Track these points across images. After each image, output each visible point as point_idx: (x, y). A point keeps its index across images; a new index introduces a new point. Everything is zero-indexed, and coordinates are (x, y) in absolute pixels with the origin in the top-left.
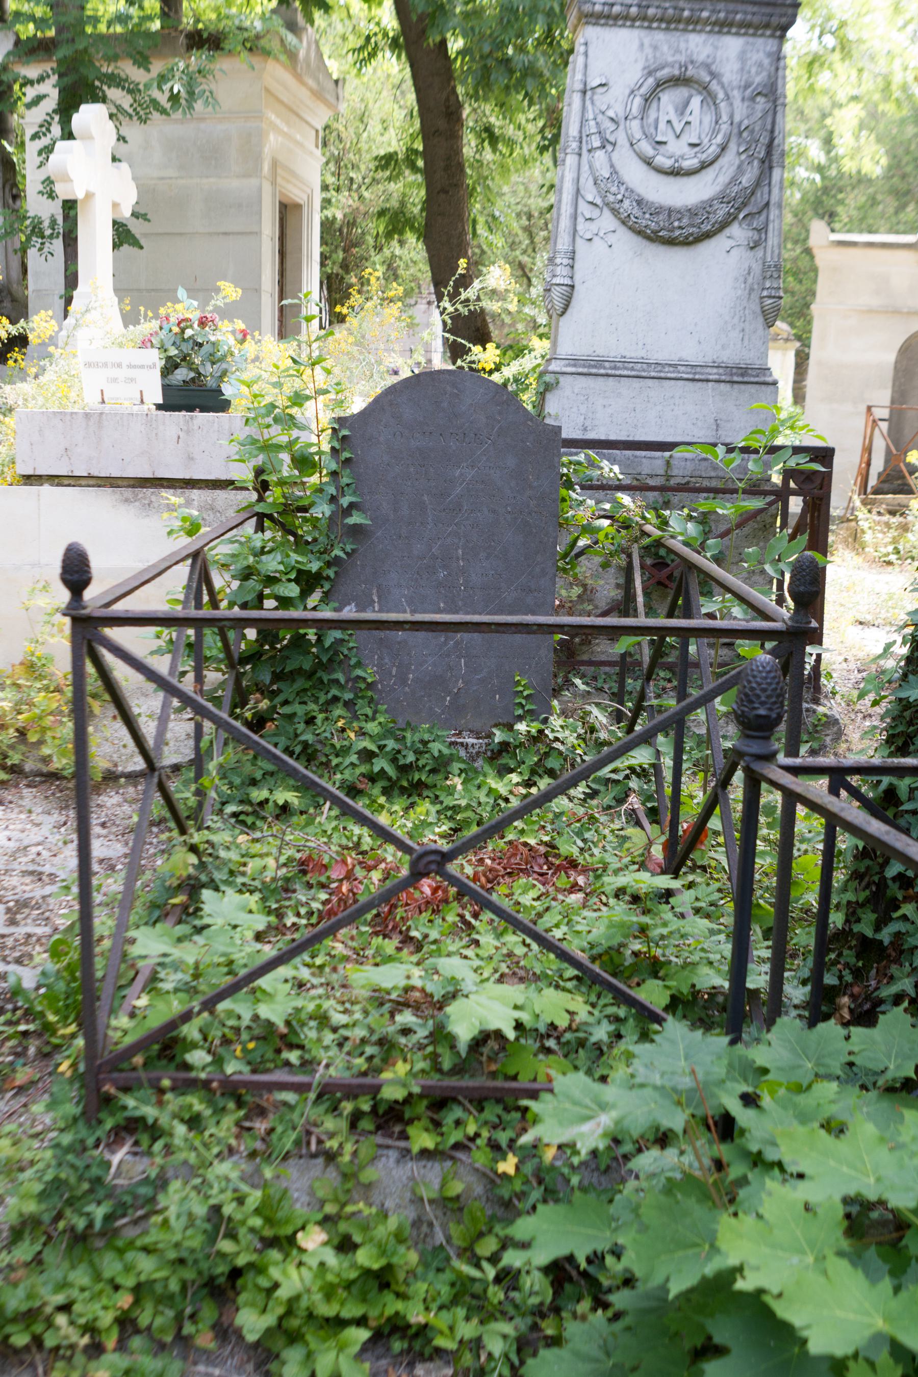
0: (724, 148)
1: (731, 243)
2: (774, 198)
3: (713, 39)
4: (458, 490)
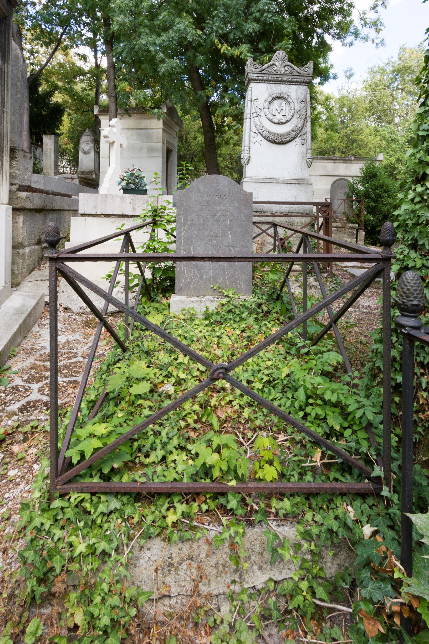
0: (293, 116)
1: (296, 143)
4: (219, 214)
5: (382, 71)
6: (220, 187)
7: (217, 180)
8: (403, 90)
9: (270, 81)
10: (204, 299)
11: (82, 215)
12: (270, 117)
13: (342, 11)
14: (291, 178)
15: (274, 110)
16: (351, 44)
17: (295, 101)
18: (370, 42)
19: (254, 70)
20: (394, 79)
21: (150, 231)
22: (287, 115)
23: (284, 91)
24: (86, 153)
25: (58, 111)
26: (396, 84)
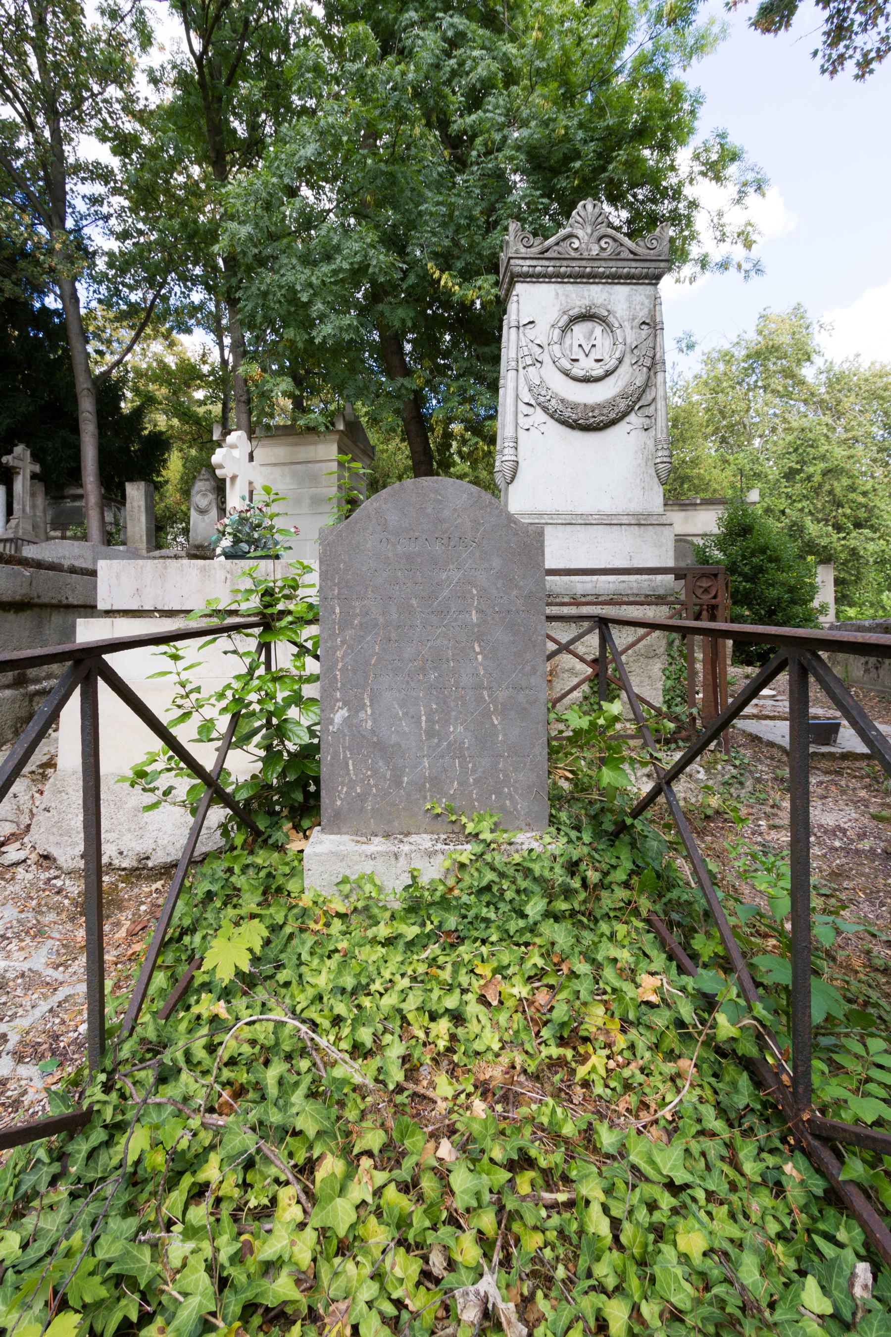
0: (620, 361)
2: (660, 393)
3: (608, 288)
4: (446, 593)
5: (727, 357)
6: (447, 513)
7: (437, 492)
8: (765, 388)
9: (563, 276)
10: (406, 848)
11: (109, 613)
12: (566, 364)
13: (675, 218)
14: (620, 511)
15: (575, 348)
16: (693, 279)
17: (626, 324)
18: (733, 270)
19: (523, 250)
20: (748, 371)
21: (251, 644)
22: (606, 358)
23: (599, 302)
24: (202, 512)
25: (158, 445)
26: (754, 378)
